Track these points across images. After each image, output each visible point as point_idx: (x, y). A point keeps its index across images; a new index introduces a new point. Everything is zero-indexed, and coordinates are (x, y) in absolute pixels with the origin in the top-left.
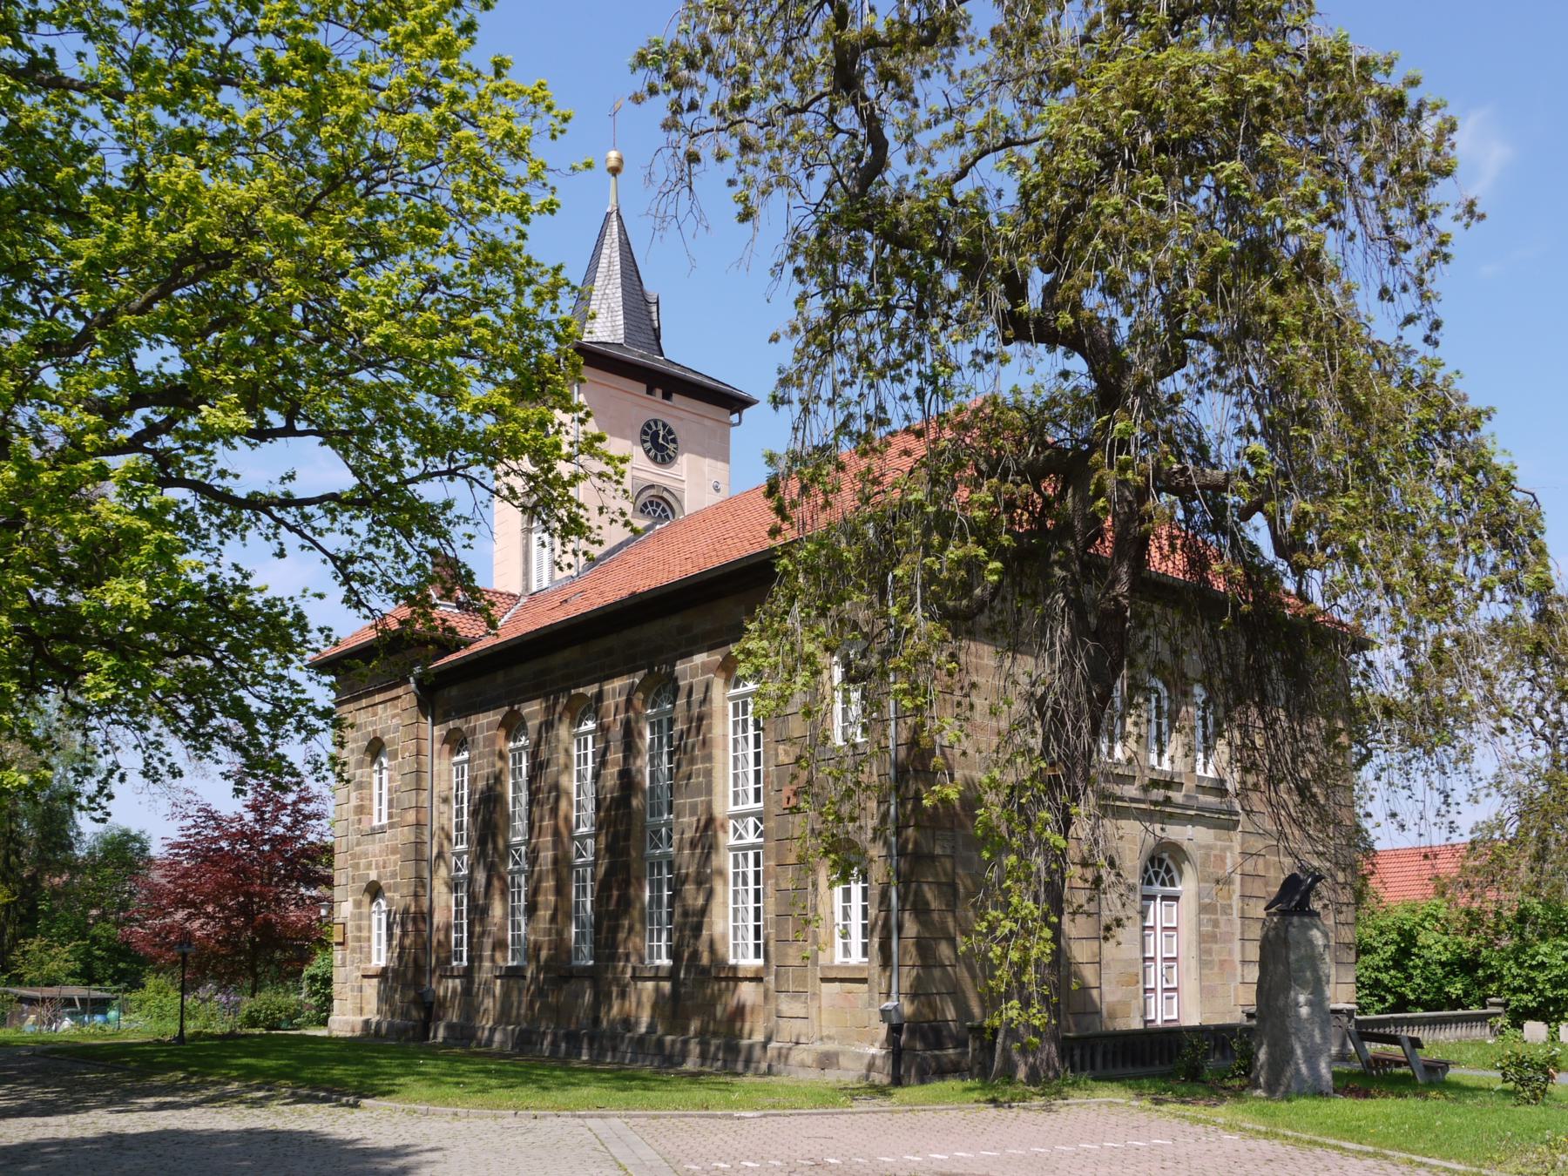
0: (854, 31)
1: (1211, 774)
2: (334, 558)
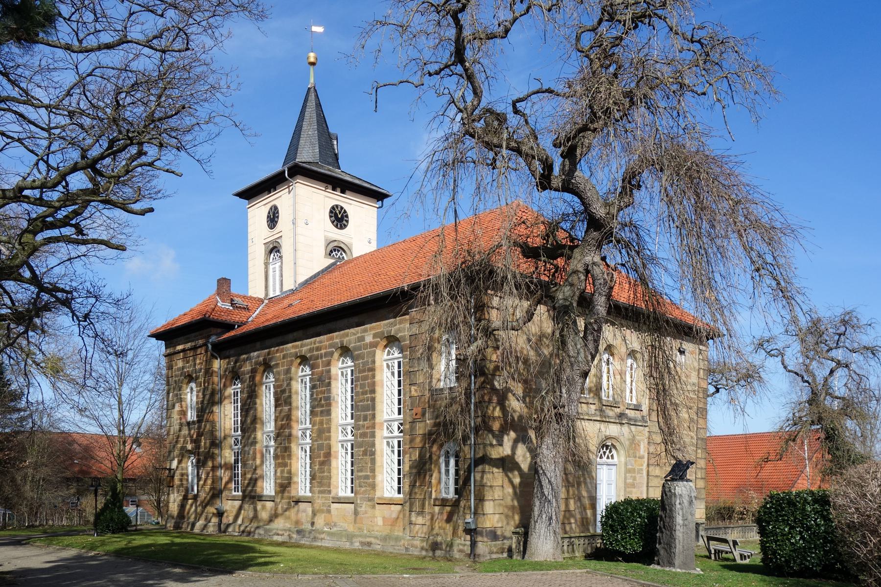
0: (780, 358)
1: (634, 402)
2: (82, 149)
